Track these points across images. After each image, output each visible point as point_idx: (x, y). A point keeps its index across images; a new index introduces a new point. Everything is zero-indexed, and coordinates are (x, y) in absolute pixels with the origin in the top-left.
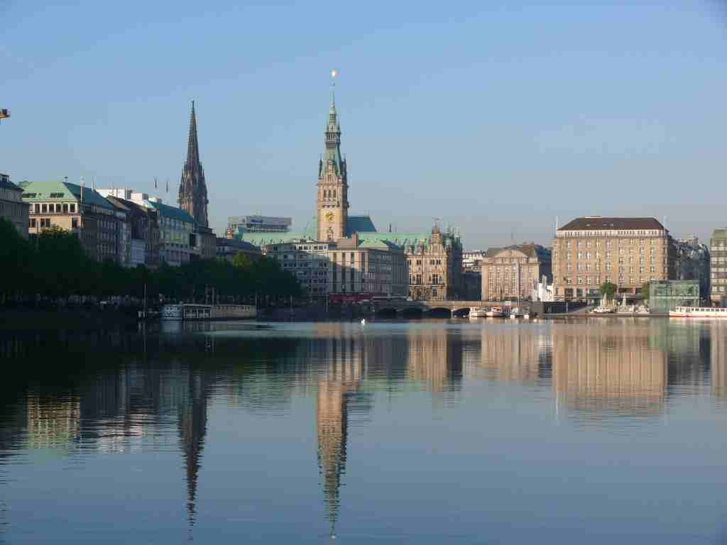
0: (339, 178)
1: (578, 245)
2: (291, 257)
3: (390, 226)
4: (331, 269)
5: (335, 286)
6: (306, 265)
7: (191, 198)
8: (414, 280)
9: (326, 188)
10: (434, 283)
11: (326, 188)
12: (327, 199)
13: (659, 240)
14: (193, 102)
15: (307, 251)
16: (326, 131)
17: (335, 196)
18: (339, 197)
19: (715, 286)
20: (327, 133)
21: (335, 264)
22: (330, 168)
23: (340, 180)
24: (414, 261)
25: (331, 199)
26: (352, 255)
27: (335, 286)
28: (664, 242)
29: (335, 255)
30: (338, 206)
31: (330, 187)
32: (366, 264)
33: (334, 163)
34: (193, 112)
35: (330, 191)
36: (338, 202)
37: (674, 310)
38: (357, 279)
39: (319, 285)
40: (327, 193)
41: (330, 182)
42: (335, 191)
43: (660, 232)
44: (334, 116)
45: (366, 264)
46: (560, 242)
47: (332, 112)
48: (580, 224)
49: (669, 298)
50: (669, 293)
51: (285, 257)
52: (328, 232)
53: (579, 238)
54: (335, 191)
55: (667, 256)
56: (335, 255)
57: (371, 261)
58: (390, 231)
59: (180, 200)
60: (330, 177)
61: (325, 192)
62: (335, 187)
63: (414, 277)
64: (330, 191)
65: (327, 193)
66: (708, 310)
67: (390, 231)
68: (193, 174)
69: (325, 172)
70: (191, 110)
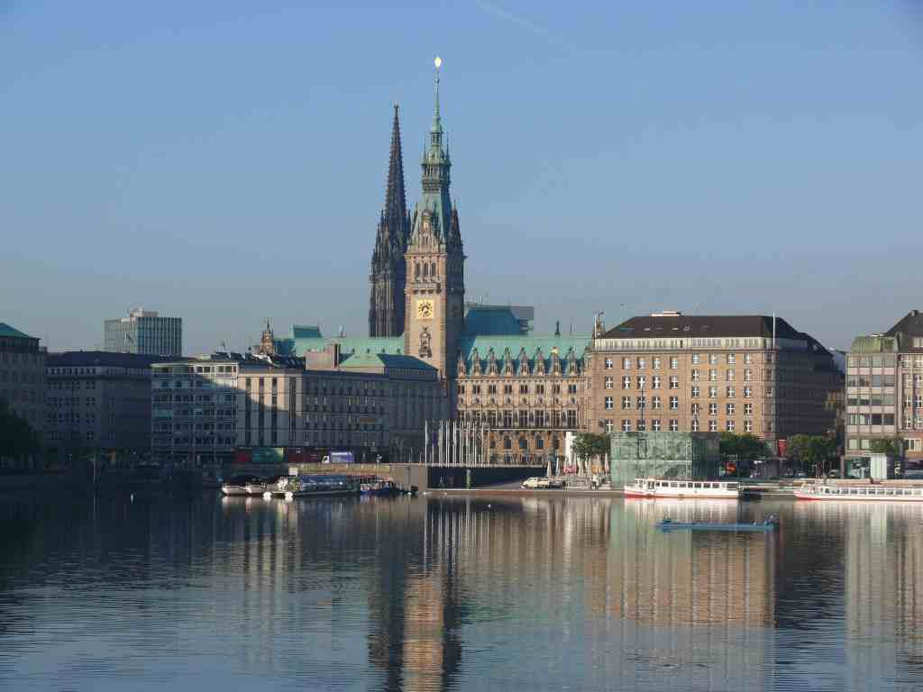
0: (441, 243)
1: (728, 361)
2: (186, 385)
3: (558, 325)
4: (242, 406)
5: (248, 436)
6: (207, 398)
7: (389, 272)
8: (564, 419)
9: (426, 259)
10: (505, 427)
11: (419, 259)
12: (428, 279)
13: (759, 355)
14: (397, 108)
15: (210, 374)
16: (422, 161)
17: (433, 273)
18: (441, 277)
19: (854, 438)
20: (425, 166)
21: (248, 400)
22: (426, 225)
23: (443, 246)
24: (469, 387)
25: (428, 279)
26: (275, 381)
27: (248, 436)
28: (769, 360)
29: (248, 382)
30: (439, 291)
31: (426, 259)
32: (299, 397)
33: (434, 217)
34: (396, 124)
35: (426, 265)
36: (439, 285)
37: (630, 484)
38: (280, 420)
39: (225, 433)
40: (422, 268)
41: (426, 250)
42: (433, 266)
43: (765, 343)
44: (438, 136)
45: (299, 397)
46: (596, 359)
47: (434, 129)
48: (637, 327)
49: (642, 462)
50: (642, 454)
51: (179, 384)
52: (421, 336)
53: (628, 352)
54: (433, 266)
55: (774, 384)
56: (248, 382)
57: (306, 392)
58: (558, 333)
59: (374, 276)
60: (425, 241)
61: (418, 266)
62: (434, 259)
63: (500, 414)
64: (426, 265)
65: (422, 268)
66: (707, 486)
67: (558, 333)
68: (392, 232)
69: (419, 233)
70: (393, 121)
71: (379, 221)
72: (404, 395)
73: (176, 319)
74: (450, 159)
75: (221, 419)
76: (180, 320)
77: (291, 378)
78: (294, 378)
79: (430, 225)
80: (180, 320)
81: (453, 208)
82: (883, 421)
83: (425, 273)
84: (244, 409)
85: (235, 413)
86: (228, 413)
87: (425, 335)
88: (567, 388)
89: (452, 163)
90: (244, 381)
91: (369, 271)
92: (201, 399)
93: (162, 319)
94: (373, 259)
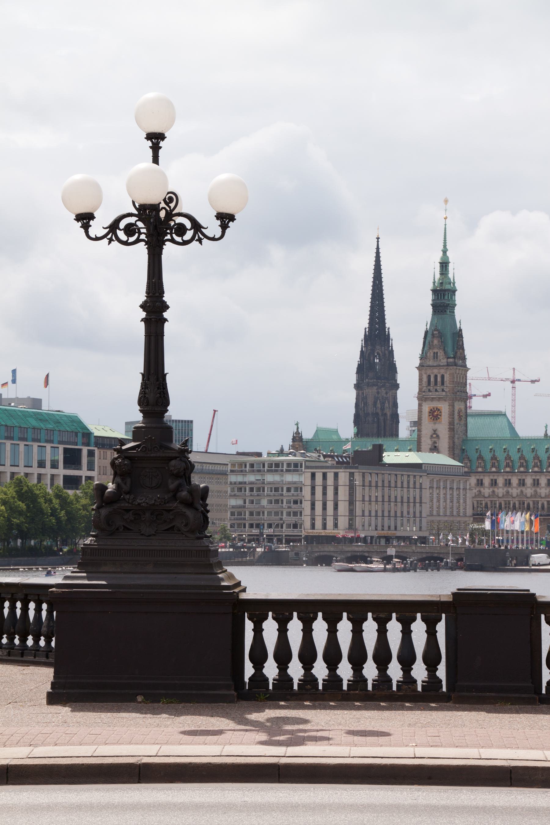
22: (436, 342)
35: (436, 377)
40: (432, 379)
54: (443, 377)
64: (436, 377)
65: (432, 379)
70: (375, 251)
71: (363, 337)
72: (438, 488)
73: (188, 421)
74: (456, 285)
75: (289, 507)
76: (192, 422)
77: (350, 473)
78: (353, 473)
79: (439, 342)
80: (192, 422)
81: (458, 326)
82: (284, 542)
83: (436, 383)
84: (321, 499)
85: (301, 503)
86: (296, 502)
87: (435, 436)
88: (517, 482)
89: (457, 288)
90: (309, 475)
91: (353, 379)
92: (271, 491)
93: (176, 421)
94: (360, 370)
